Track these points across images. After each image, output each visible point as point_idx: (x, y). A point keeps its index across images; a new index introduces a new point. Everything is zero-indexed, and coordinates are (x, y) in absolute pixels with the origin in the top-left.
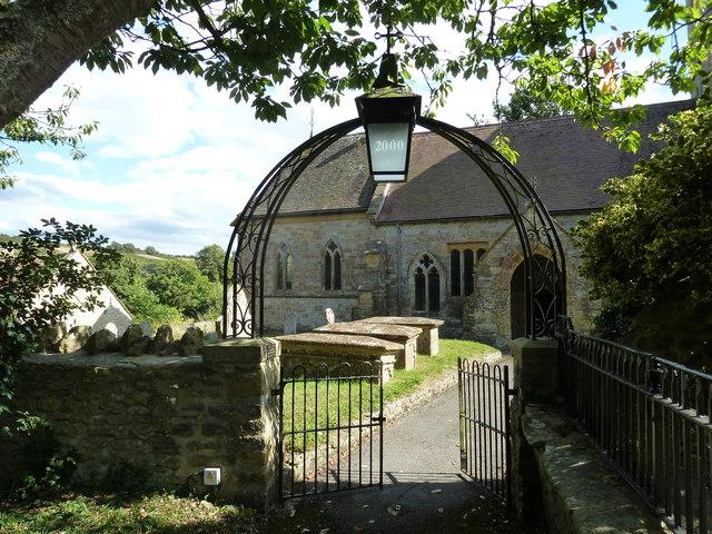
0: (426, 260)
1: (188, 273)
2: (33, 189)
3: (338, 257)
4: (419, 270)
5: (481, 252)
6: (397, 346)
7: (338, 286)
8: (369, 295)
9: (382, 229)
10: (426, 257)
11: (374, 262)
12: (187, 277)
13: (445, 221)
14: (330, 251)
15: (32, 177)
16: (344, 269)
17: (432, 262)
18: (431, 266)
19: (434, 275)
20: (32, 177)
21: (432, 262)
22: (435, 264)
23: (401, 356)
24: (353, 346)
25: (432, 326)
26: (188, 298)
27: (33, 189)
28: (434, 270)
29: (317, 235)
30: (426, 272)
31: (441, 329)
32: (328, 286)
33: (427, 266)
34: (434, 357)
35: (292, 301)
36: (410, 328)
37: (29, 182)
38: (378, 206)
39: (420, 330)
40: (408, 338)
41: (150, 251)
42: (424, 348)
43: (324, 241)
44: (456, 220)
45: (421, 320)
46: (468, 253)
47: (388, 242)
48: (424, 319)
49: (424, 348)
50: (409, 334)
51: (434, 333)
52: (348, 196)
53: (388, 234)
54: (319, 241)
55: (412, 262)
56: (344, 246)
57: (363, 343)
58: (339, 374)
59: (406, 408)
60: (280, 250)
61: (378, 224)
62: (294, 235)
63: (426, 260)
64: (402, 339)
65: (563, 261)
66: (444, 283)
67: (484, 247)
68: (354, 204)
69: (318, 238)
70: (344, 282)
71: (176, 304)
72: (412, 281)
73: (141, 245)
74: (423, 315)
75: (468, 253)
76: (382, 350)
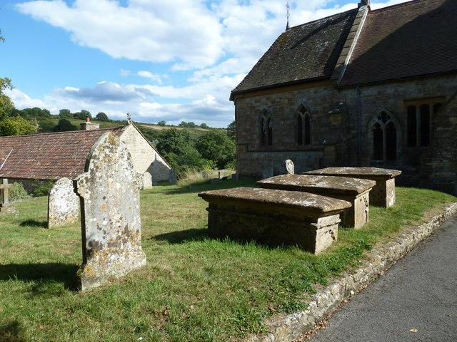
0: (384, 116)
1: (220, 138)
2: (139, 93)
3: (307, 118)
4: (377, 125)
5: (438, 107)
6: (342, 204)
7: (308, 142)
8: (332, 148)
9: (344, 92)
10: (383, 113)
11: (336, 121)
12: (219, 140)
13: (402, 80)
14: (301, 114)
15: (137, 87)
16: (312, 128)
17: (389, 117)
18: (388, 121)
19: (391, 128)
20: (137, 87)
21: (389, 117)
22: (392, 120)
23: (347, 218)
24: (284, 205)
25: (389, 177)
26: (220, 154)
27: (139, 93)
28: (391, 125)
29: (291, 102)
30: (383, 126)
31: (397, 178)
32: (300, 143)
33: (384, 121)
34: (390, 209)
35: (273, 155)
36: (361, 181)
37: (136, 90)
38: (339, 73)
39: (374, 183)
40: (357, 194)
41: (203, 126)
42: (378, 199)
43: (296, 107)
44: (412, 78)
45: (375, 171)
46: (425, 109)
47: (349, 102)
48: (380, 170)
49: (378, 199)
50: (359, 188)
51: (390, 183)
52: (315, 68)
53: (350, 96)
54: (293, 107)
55: (370, 119)
56: (312, 109)
57: (296, 202)
58: (268, 240)
59: (347, 293)
60: (263, 116)
61: (340, 89)
62: (273, 102)
63: (384, 116)
64: (351, 195)
65: (311, 174)
66: (400, 136)
67: (441, 101)
68: (319, 73)
69: (291, 105)
70: (312, 138)
71: (213, 158)
72: (370, 135)
73: (198, 123)
74: (380, 165)
75: (425, 109)
76: (318, 212)
